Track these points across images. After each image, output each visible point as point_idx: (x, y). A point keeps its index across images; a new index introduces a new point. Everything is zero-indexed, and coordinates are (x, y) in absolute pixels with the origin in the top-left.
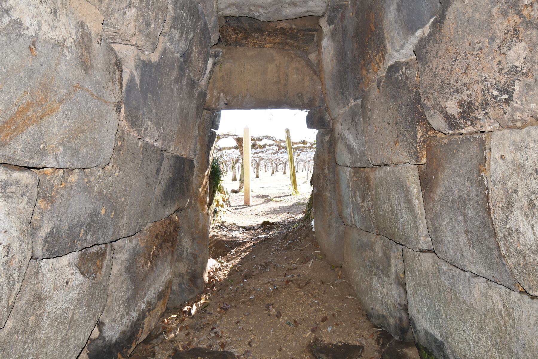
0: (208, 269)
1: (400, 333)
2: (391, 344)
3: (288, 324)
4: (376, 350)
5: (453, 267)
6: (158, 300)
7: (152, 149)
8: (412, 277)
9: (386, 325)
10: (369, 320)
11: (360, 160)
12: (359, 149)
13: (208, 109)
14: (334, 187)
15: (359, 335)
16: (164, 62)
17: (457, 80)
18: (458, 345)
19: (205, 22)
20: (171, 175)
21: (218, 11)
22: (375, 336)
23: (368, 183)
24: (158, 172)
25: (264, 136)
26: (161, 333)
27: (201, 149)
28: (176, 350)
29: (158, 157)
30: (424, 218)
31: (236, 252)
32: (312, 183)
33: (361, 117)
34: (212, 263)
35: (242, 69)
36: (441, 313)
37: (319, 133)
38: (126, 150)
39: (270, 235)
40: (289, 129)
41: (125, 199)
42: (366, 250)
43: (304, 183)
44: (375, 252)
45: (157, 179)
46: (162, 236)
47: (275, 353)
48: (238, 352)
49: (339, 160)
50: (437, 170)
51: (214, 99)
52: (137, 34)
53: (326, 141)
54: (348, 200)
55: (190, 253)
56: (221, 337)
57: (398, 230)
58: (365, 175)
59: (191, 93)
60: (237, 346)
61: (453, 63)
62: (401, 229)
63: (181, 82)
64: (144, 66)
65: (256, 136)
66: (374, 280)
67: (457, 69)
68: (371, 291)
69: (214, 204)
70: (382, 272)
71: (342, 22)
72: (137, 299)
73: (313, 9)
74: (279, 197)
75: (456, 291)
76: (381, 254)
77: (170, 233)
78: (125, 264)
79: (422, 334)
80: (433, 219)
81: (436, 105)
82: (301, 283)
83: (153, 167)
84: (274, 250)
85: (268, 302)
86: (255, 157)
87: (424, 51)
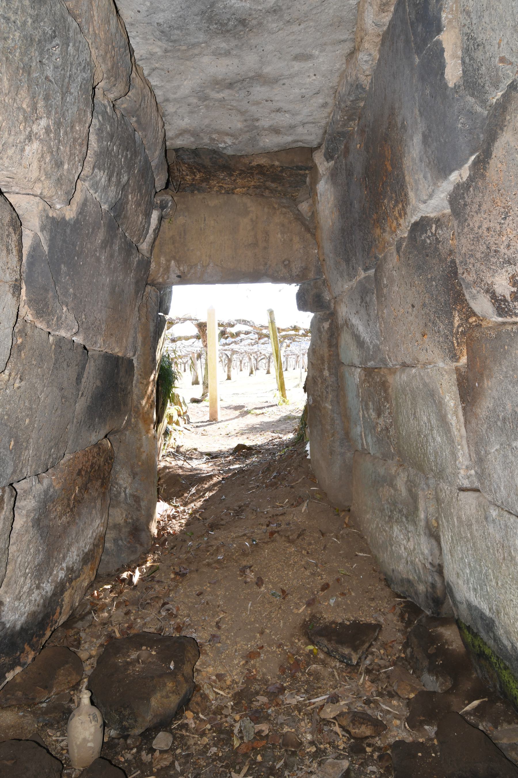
0: (157, 517)
1: (432, 605)
2: (420, 621)
3: (273, 595)
4: (399, 631)
5: (506, 513)
6: (83, 565)
7: (69, 346)
8: (448, 526)
9: (413, 594)
10: (389, 586)
11: (373, 358)
12: (371, 342)
13: (153, 284)
14: (337, 396)
15: (375, 609)
16: (85, 219)
17: (508, 246)
18: (514, 623)
19: (146, 157)
20: (98, 383)
21: (164, 141)
22: (398, 610)
23: (386, 391)
24: (79, 379)
25: (237, 321)
26: (89, 613)
27: (144, 343)
28: (110, 637)
29: (79, 358)
30: (464, 442)
31: (198, 491)
32: (305, 389)
33: (375, 295)
34: (162, 508)
35: (202, 226)
36: (489, 578)
37: (315, 317)
38: (29, 350)
39: (247, 465)
40: (273, 309)
41: (30, 421)
42: (383, 486)
43: (296, 387)
44: (396, 490)
45: (78, 390)
46: (87, 471)
47: (255, 637)
48: (201, 638)
49: (343, 357)
50: (482, 374)
51: (161, 269)
52: (42, 179)
53: (326, 328)
54: (358, 414)
55: (130, 495)
56: (176, 616)
57: (428, 458)
58: (381, 379)
59: (126, 262)
60: (200, 628)
61: (503, 221)
62: (432, 458)
63: (111, 247)
64: (55, 226)
65: (226, 321)
66: (396, 529)
67: (509, 230)
68: (391, 545)
69: (165, 420)
70: (407, 518)
71: (345, 157)
72: (52, 565)
73: (304, 138)
74: (260, 408)
75: (510, 547)
76: (404, 492)
77: (99, 467)
78: (32, 515)
79: (463, 607)
80: (478, 443)
81: (479, 281)
82: (292, 535)
83: (71, 373)
84: (253, 488)
85: (244, 563)
86: (226, 350)
87: (462, 202)
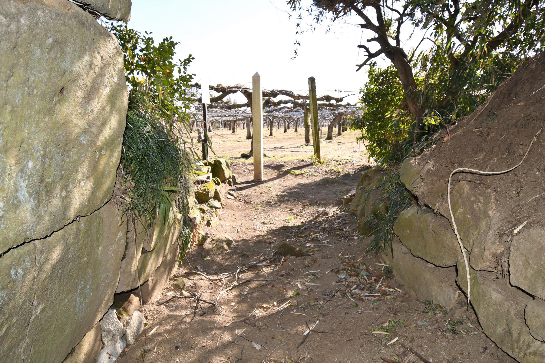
86: (269, 116)
